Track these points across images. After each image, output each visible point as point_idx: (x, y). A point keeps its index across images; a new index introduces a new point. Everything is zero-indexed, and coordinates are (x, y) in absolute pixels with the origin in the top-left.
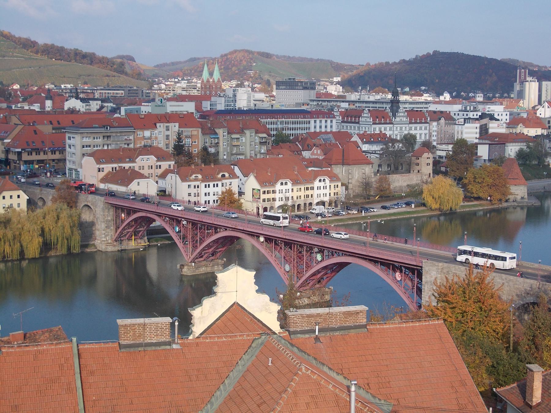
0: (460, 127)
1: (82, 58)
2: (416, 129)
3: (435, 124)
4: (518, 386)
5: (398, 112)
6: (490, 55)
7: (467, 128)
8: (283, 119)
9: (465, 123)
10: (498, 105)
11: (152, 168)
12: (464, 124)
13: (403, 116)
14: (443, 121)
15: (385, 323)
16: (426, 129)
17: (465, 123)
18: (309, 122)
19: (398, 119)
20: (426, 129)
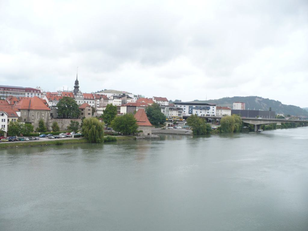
0: (111, 101)
1: (117, 141)
2: (90, 103)
3: (98, 100)
4: (4, 132)
5: (77, 92)
6: (242, 96)
7: (114, 101)
8: (8, 91)
9: (114, 99)
10: (176, 105)
11: (5, 121)
12: (113, 99)
13: (80, 95)
14: (102, 99)
15: (93, 157)
16: (93, 103)
17: (114, 99)
18: (25, 94)
19: (78, 96)
20: (93, 103)
